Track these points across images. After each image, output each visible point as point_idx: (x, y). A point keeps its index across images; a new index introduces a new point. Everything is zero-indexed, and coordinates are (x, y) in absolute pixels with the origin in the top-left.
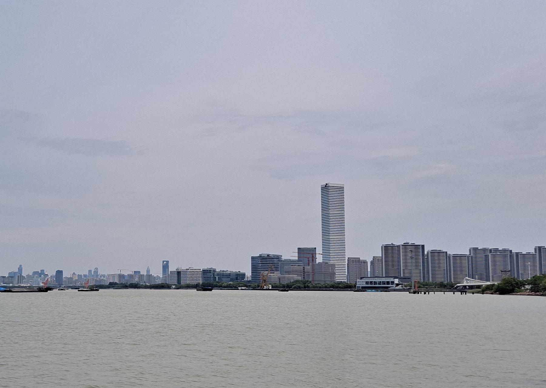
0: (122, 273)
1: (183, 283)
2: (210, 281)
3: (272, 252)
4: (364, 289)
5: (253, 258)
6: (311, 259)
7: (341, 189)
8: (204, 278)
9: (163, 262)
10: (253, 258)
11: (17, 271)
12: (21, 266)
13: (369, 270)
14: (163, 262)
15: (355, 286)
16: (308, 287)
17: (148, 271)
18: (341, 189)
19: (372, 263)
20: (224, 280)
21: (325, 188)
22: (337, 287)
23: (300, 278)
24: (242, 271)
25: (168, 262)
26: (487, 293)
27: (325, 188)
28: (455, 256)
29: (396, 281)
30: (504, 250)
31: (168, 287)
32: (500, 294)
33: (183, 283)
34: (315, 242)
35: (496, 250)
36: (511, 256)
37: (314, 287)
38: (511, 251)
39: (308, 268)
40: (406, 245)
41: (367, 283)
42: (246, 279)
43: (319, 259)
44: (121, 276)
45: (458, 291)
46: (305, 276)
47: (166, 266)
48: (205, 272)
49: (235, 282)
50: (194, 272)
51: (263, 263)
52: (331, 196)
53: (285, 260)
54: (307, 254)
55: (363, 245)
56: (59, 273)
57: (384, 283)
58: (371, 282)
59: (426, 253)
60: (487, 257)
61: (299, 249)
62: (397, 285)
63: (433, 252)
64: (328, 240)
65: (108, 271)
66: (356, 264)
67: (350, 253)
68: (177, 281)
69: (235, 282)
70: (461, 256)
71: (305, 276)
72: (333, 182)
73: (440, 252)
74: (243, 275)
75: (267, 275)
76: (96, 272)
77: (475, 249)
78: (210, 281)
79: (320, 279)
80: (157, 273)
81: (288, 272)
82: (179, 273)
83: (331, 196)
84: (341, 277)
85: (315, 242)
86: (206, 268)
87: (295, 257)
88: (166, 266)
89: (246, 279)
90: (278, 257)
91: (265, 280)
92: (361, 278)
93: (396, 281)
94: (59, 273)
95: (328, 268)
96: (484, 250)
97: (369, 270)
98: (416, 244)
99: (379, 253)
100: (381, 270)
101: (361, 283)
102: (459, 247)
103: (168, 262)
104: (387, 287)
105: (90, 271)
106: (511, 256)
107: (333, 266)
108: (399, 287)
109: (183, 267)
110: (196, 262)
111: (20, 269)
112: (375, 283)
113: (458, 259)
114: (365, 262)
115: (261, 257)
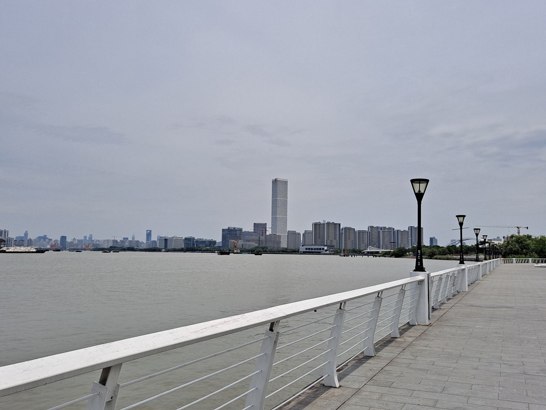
0: (116, 239)
1: (169, 247)
2: (192, 246)
3: (237, 226)
4: (304, 253)
5: (223, 230)
6: (264, 232)
7: (285, 183)
8: (186, 244)
9: (147, 231)
10: (223, 230)
11: (23, 236)
12: (26, 231)
13: (302, 239)
14: (147, 231)
15: (298, 251)
16: (266, 251)
17: (133, 238)
18: (285, 183)
19: (304, 235)
20: (201, 245)
21: (275, 182)
22: (286, 252)
23: (257, 245)
24: (214, 239)
25: (151, 231)
26: (436, 259)
27: (275, 182)
28: (359, 232)
29: (326, 248)
30: (390, 228)
31: (159, 250)
32: (396, 257)
33: (169, 247)
34: (266, 219)
35: (385, 228)
36: (394, 232)
37: (270, 251)
38: (394, 229)
39: (263, 238)
40: (328, 224)
41: (306, 249)
42: (217, 245)
43: (269, 232)
44: (115, 241)
45: (365, 255)
46: (261, 244)
47: (149, 235)
48: (186, 239)
49: (207, 247)
50: (177, 240)
51: (230, 234)
52: (279, 187)
53: (245, 232)
54: (260, 227)
55: (299, 223)
56: (63, 238)
57: (317, 249)
58: (309, 249)
59: (341, 228)
60: (379, 232)
61: (255, 224)
62: (326, 250)
63: (346, 229)
64: (276, 218)
65: (104, 236)
66: (293, 235)
67: (290, 227)
68: (166, 246)
69: (207, 247)
70: (364, 232)
71: (261, 244)
72: (281, 177)
73: (350, 229)
74: (215, 242)
75: (231, 242)
76: (91, 237)
77: (372, 227)
78: (192, 246)
79: (270, 246)
80: (142, 239)
81: (249, 241)
82: (166, 240)
83: (279, 187)
84: (284, 245)
85: (266, 219)
86: (187, 237)
87: (251, 229)
88: (149, 235)
89: (217, 245)
90: (241, 230)
91: (235, 247)
92: (303, 246)
93: (326, 248)
94: (63, 238)
95: (275, 238)
96: (377, 228)
97: (302, 239)
98: (335, 223)
99: (310, 228)
100: (311, 239)
101: (302, 249)
102: (361, 226)
103: (151, 231)
104: (320, 252)
105: (85, 237)
106: (394, 232)
107: (280, 236)
108: (328, 252)
109: (169, 236)
110: (181, 232)
111: (26, 234)
112: (312, 249)
113: (361, 233)
114: (299, 234)
115: (229, 230)
